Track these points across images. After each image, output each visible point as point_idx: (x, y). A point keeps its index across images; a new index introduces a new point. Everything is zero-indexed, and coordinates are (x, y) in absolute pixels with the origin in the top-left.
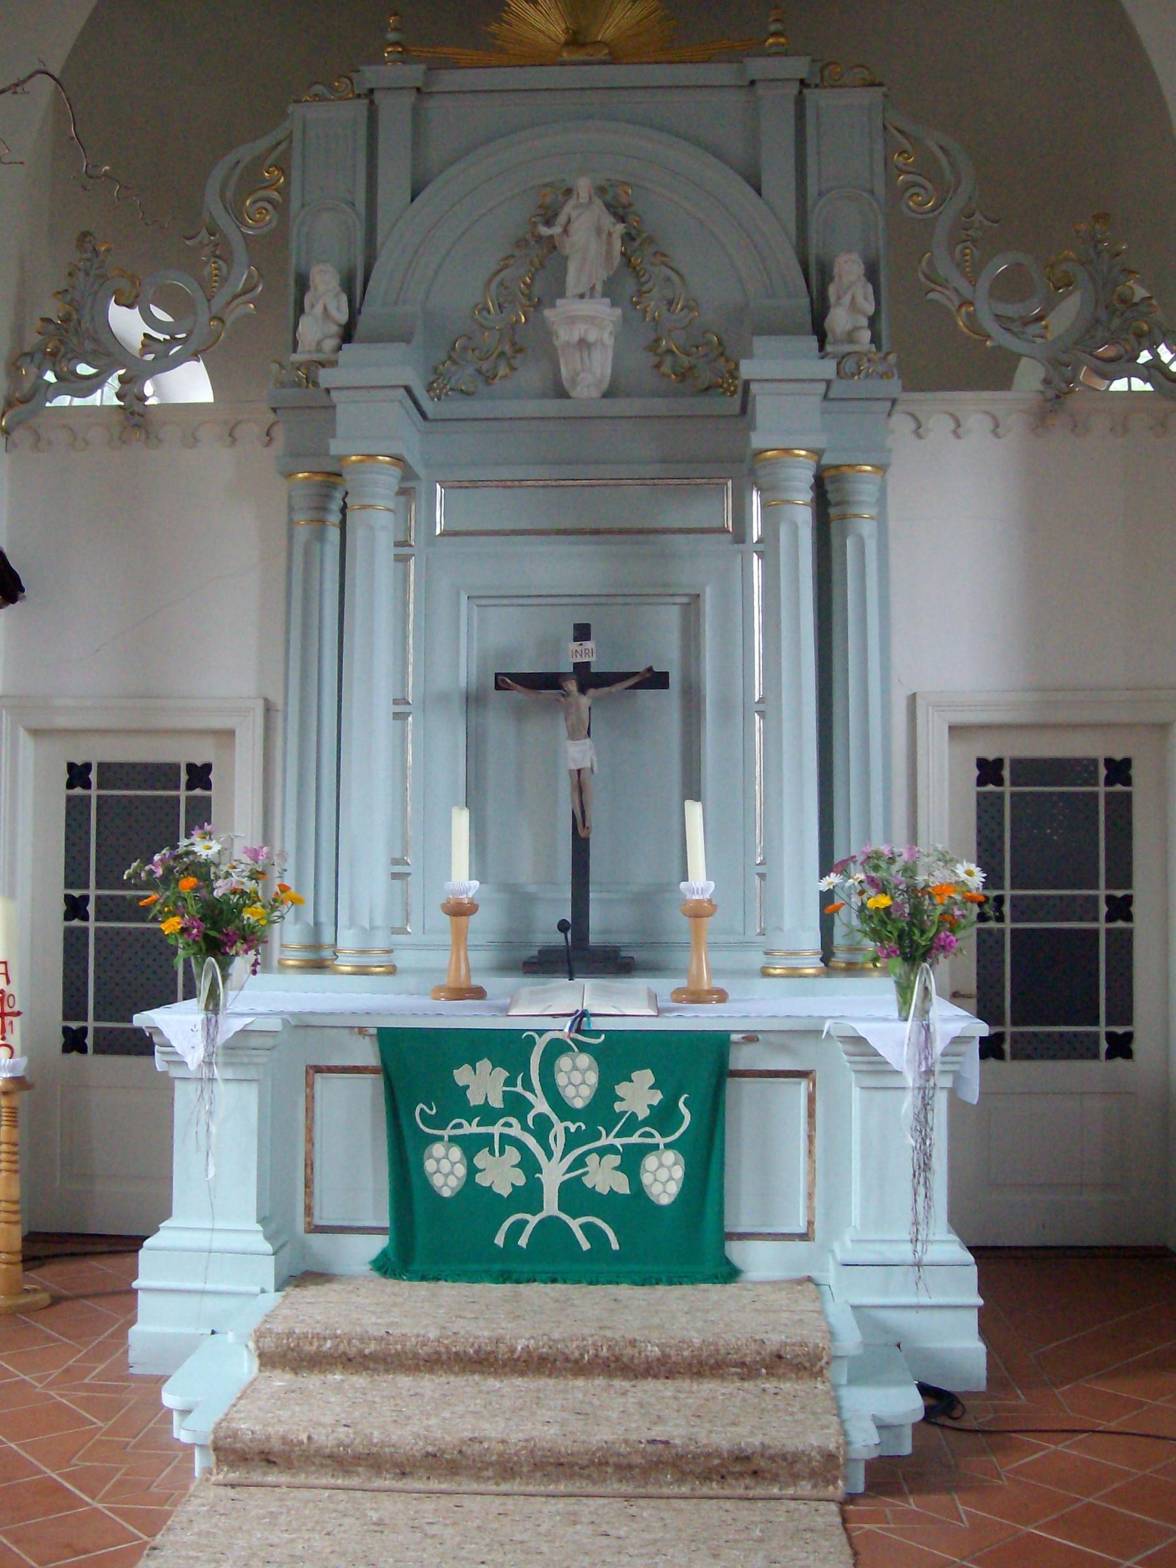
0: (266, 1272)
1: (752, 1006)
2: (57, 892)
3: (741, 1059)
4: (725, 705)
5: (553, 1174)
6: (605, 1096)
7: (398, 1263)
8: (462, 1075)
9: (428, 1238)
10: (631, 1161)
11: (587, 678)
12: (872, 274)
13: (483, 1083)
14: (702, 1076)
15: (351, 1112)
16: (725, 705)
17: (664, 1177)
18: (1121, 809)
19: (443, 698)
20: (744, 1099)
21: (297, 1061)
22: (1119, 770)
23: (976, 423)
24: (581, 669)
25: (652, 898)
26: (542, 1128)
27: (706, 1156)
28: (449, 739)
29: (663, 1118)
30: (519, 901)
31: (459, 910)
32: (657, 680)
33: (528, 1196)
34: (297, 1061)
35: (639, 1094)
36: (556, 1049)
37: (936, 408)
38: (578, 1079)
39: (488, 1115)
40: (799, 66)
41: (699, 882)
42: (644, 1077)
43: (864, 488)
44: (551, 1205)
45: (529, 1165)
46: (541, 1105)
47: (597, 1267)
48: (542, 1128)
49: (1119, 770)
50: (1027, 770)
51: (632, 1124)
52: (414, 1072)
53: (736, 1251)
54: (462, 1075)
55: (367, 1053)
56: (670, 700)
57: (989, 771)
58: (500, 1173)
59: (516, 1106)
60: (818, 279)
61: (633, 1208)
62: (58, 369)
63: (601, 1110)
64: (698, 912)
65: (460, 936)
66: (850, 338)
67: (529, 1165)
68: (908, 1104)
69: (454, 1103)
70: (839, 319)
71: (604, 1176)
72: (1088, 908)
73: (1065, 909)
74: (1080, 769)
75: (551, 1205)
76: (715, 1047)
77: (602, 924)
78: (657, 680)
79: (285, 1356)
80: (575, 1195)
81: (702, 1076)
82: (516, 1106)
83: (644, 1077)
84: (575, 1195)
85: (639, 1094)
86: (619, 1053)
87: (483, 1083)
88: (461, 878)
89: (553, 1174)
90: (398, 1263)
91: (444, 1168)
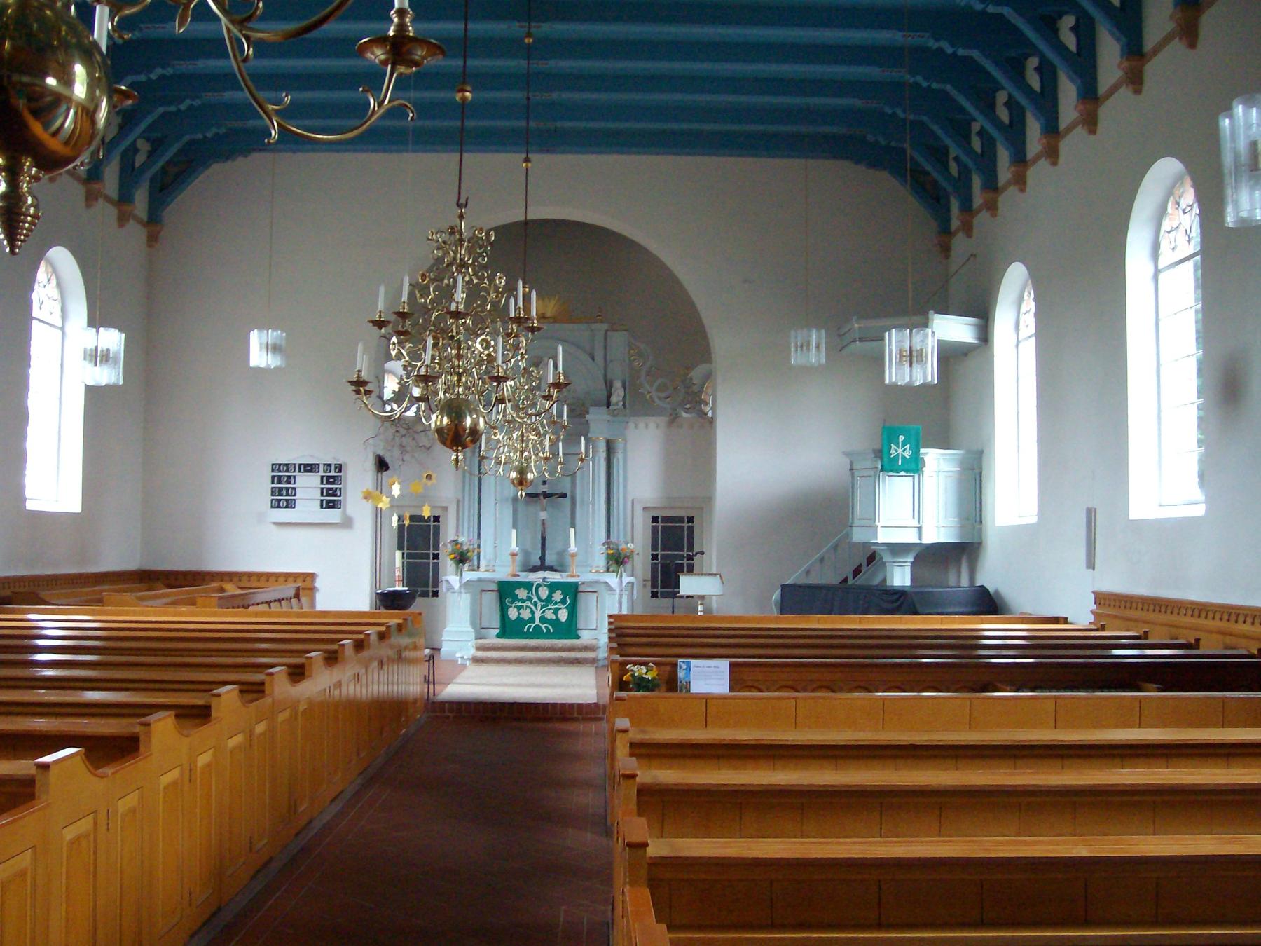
0: (473, 636)
1: (585, 576)
2: (650, 552)
3: (581, 588)
4: (582, 501)
5: (538, 615)
6: (550, 596)
7: (501, 635)
8: (517, 592)
9: (508, 628)
10: (556, 611)
11: (546, 495)
12: (624, 386)
13: (522, 593)
14: (573, 592)
15: (490, 601)
16: (582, 501)
17: (563, 615)
18: (691, 530)
19: (507, 500)
20: (582, 597)
21: (477, 588)
22: (691, 520)
23: (652, 426)
24: (544, 492)
25: (562, 554)
26: (535, 604)
27: (573, 611)
28: (508, 512)
29: (563, 601)
30: (526, 554)
31: (514, 555)
32: (564, 496)
33: (532, 620)
34: (477, 588)
35: (558, 596)
36: (539, 586)
37: (641, 422)
38: (544, 592)
39: (523, 601)
40: (605, 326)
41: (573, 548)
42: (559, 592)
43: (620, 445)
44: (537, 622)
45: (532, 612)
46: (535, 599)
47: (548, 635)
48: (535, 604)
49: (691, 520)
50: (666, 519)
51: (556, 603)
52: (505, 591)
53: (580, 633)
54: (517, 592)
55: (494, 587)
56: (567, 501)
57: (655, 519)
58: (526, 615)
59: (529, 599)
60: (609, 385)
61: (556, 623)
62: (87, 125)
63: (549, 600)
64: (573, 556)
65: (514, 561)
66: (617, 404)
67: (532, 612)
68: (617, 597)
69: (515, 598)
70: (614, 399)
71: (550, 615)
72: (682, 557)
73: (677, 557)
74: (681, 519)
75: (537, 622)
76: (576, 584)
77: (550, 559)
78: (564, 496)
79: (478, 649)
80: (543, 620)
81: (573, 592)
82: (529, 599)
83: (559, 592)
84: (543, 620)
85: (558, 596)
86: (553, 587)
87: (522, 593)
88: (514, 547)
89: (538, 615)
90: (501, 635)
91: (513, 614)
